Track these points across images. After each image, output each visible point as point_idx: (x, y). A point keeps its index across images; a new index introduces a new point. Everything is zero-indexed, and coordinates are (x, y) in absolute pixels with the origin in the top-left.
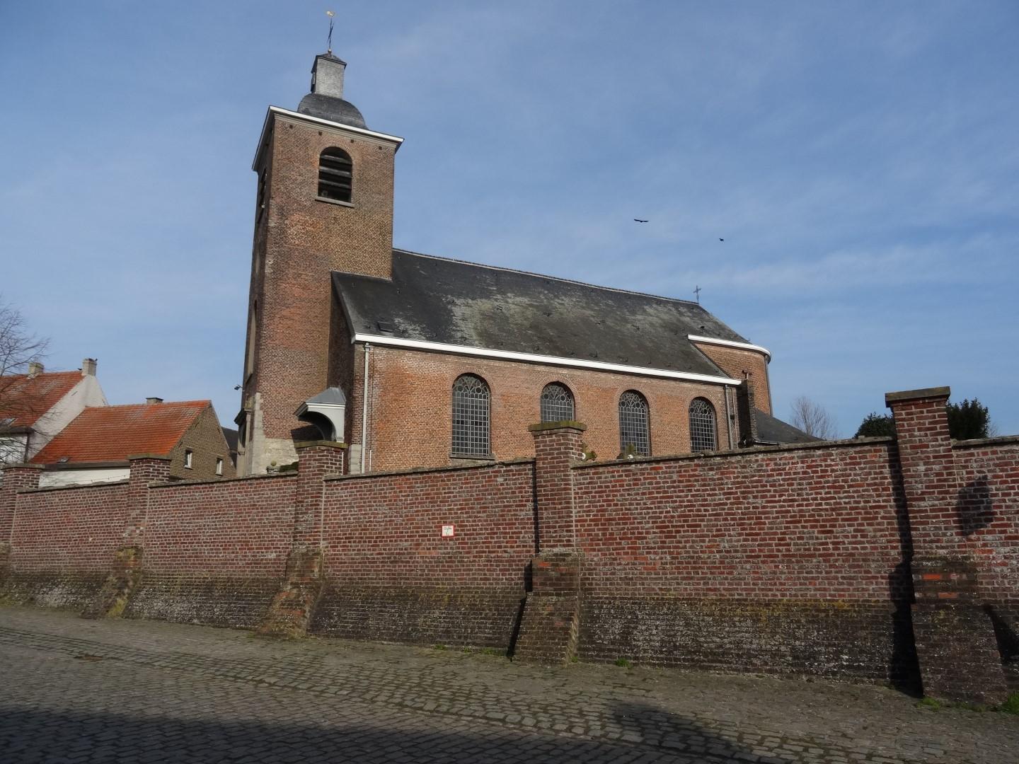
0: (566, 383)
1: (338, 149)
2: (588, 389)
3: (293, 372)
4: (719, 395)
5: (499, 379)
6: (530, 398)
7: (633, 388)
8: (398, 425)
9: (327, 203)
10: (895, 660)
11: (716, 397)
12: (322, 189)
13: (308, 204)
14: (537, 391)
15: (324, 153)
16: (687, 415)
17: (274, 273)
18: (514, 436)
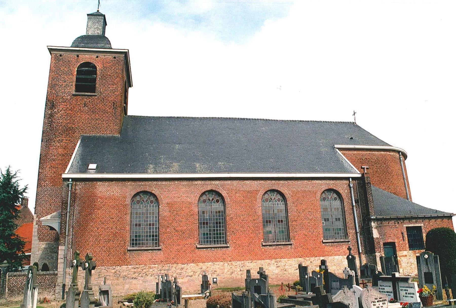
0: (218, 190)
2: (236, 193)
4: (345, 186)
5: (165, 193)
7: (273, 188)
11: (342, 187)
12: (78, 88)
14: (193, 198)
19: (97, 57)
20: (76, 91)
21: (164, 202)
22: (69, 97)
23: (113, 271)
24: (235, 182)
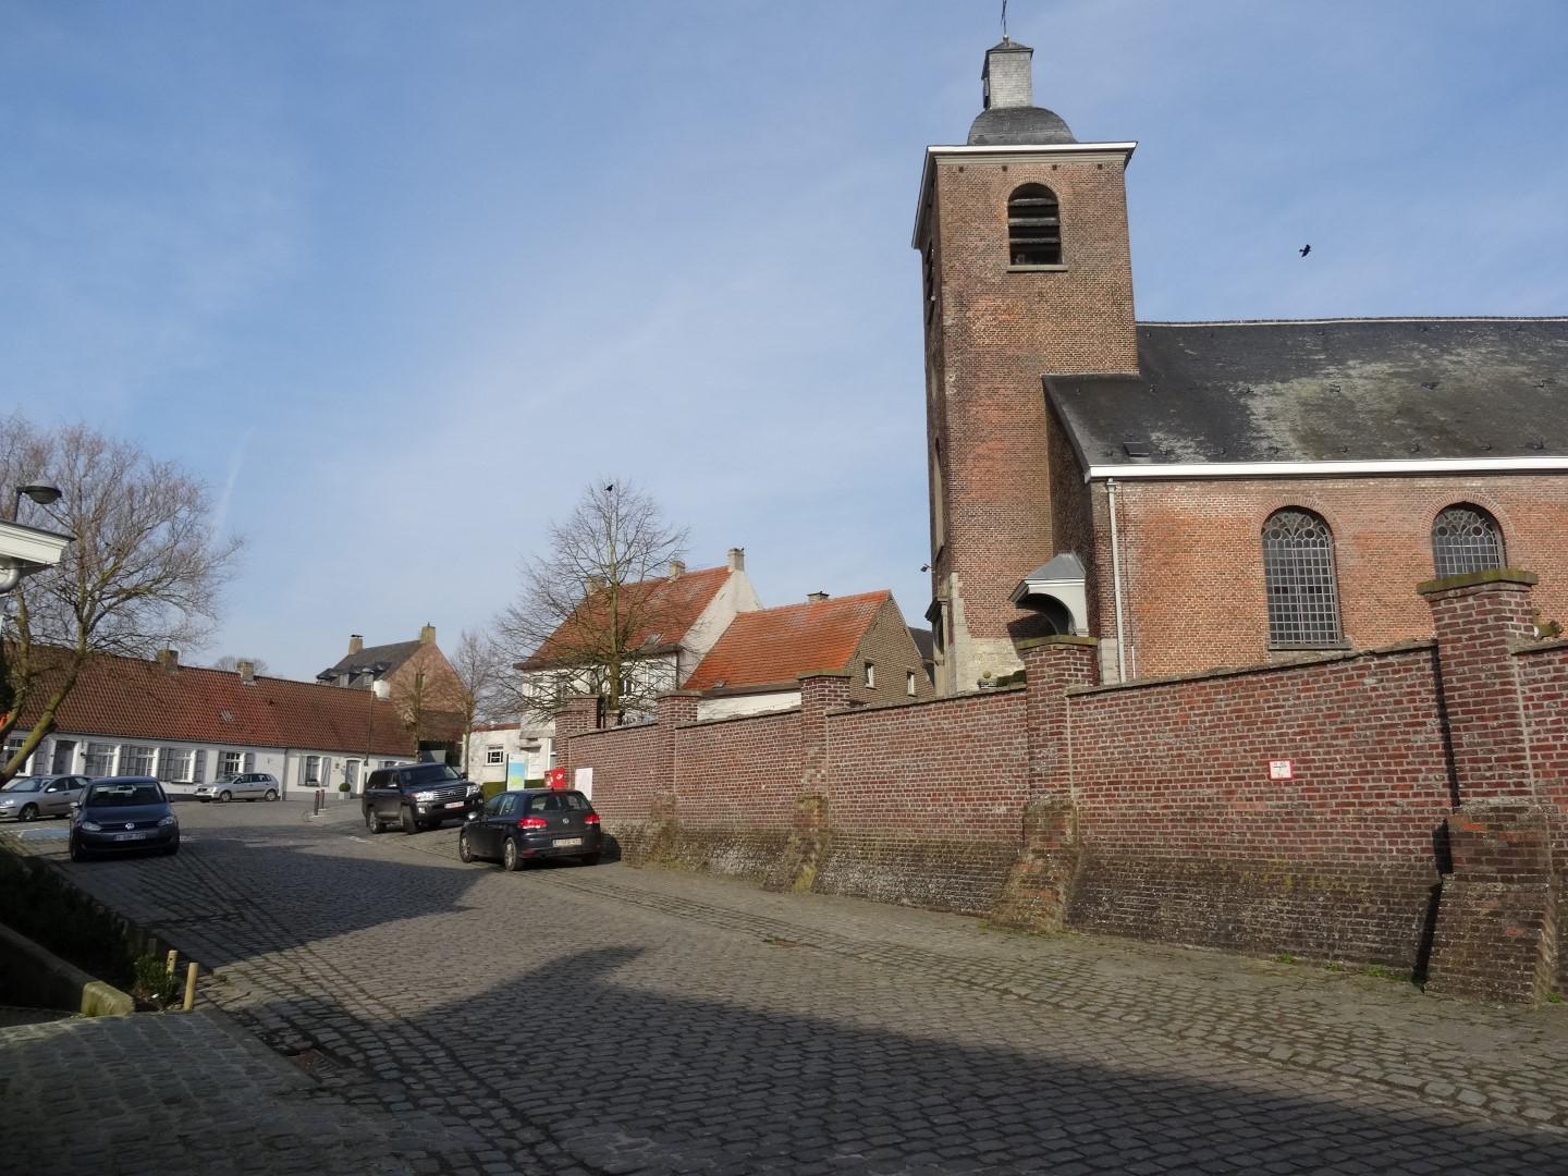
2: (1530, 509)
3: (1000, 538)
6: (1410, 537)
8: (1174, 603)
12: (1016, 253)
13: (997, 280)
14: (1423, 525)
15: (1012, 198)
17: (958, 393)
19: (1055, 168)
20: (1013, 263)
21: (1345, 533)
22: (997, 280)
24: (1524, 481)
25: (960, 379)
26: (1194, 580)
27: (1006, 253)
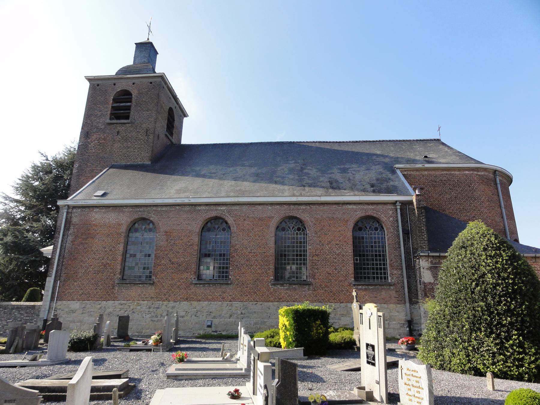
1: (126, 91)
2: (245, 220)
4: (391, 212)
6: (190, 232)
8: (82, 261)
9: (114, 124)
10: (70, 360)
13: (103, 127)
14: (196, 226)
16: (350, 234)
17: (78, 172)
18: (173, 263)
19: (134, 84)
20: (111, 119)
21: (162, 230)
22: (103, 127)
23: (99, 306)
24: (245, 208)
25: (80, 166)
26: (92, 251)
27: (108, 116)
